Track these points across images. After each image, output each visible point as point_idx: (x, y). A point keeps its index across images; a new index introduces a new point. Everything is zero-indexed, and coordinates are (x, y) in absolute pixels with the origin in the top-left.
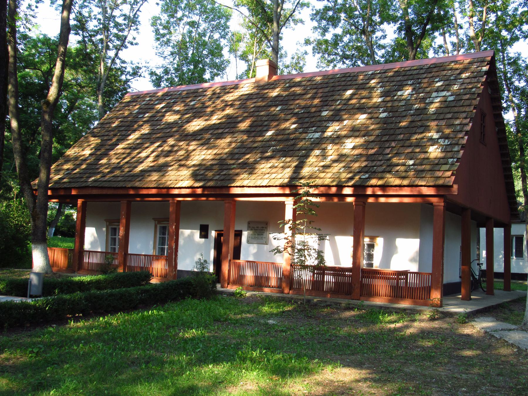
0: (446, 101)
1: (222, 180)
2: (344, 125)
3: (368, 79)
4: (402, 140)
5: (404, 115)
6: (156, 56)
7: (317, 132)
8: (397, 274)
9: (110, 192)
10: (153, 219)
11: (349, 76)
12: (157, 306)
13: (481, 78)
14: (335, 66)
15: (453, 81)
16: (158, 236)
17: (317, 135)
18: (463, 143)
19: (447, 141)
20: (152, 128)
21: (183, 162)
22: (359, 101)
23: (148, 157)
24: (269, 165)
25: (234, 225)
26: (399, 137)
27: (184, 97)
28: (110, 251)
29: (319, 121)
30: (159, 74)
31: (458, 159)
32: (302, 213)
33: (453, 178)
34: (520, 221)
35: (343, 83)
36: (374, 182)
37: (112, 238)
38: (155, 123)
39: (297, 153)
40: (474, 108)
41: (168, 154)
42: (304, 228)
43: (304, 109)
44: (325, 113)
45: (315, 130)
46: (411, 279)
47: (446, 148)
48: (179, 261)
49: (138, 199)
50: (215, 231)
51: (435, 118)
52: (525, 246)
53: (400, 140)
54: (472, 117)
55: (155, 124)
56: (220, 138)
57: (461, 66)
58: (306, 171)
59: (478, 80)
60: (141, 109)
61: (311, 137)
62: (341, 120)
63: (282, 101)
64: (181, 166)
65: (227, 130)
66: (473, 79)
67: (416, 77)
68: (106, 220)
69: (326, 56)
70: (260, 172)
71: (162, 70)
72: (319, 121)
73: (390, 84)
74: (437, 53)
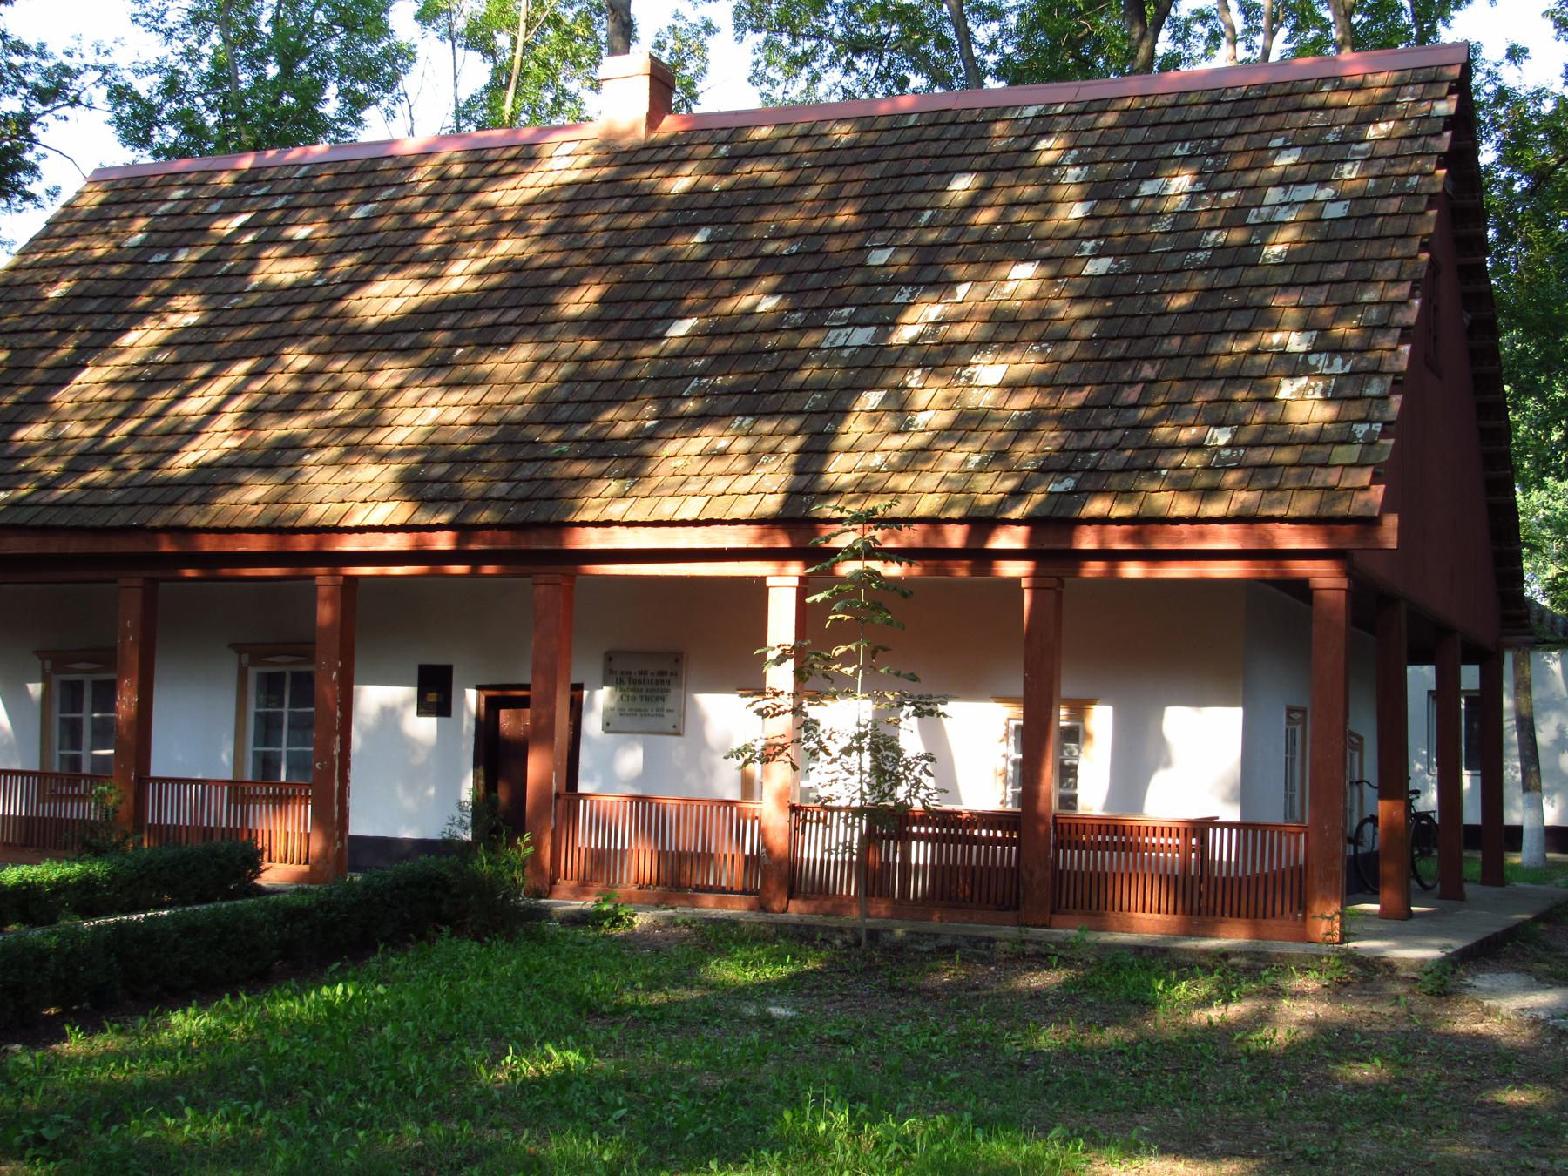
0: (1319, 220)
1: (522, 500)
2: (959, 299)
3: (1024, 135)
4: (1178, 356)
5: (1175, 265)
6: (137, 26)
7: (863, 325)
8: (1182, 833)
9: (75, 546)
10: (231, 646)
11: (953, 123)
12: (343, 968)
13: (1433, 141)
14: (815, 79)
15: (1335, 147)
16: (252, 709)
17: (861, 336)
18: (1396, 369)
19: (1338, 361)
20: (212, 305)
21: (356, 437)
22: (1003, 215)
23: (215, 412)
24: (697, 444)
25: (569, 667)
26: (1165, 346)
27: (324, 187)
28: (57, 769)
29: (862, 285)
30: (144, 94)
31: (1386, 424)
32: (847, 617)
33: (1378, 491)
34: (1531, 638)
35: (934, 148)
36: (1097, 507)
37: (63, 720)
38: (221, 285)
39: (794, 402)
40: (1424, 247)
41: (289, 406)
42: (856, 673)
43: (800, 240)
44: (879, 257)
45: (851, 315)
46: (1223, 846)
47: (1337, 388)
48: (354, 802)
49: (190, 573)
50: (479, 688)
51: (1287, 278)
53: (1172, 358)
54: (1416, 276)
55: (219, 289)
56: (490, 344)
57: (1358, 98)
58: (840, 469)
59: (1423, 147)
60: (156, 231)
61: (840, 342)
62: (944, 285)
63: (710, 208)
64: (351, 449)
65: (511, 316)
66: (1407, 143)
67: (1199, 129)
68: (43, 654)
69: (786, 40)
70: (665, 469)
71: (155, 80)
72: (862, 285)
73: (1110, 152)
74: (1182, 40)
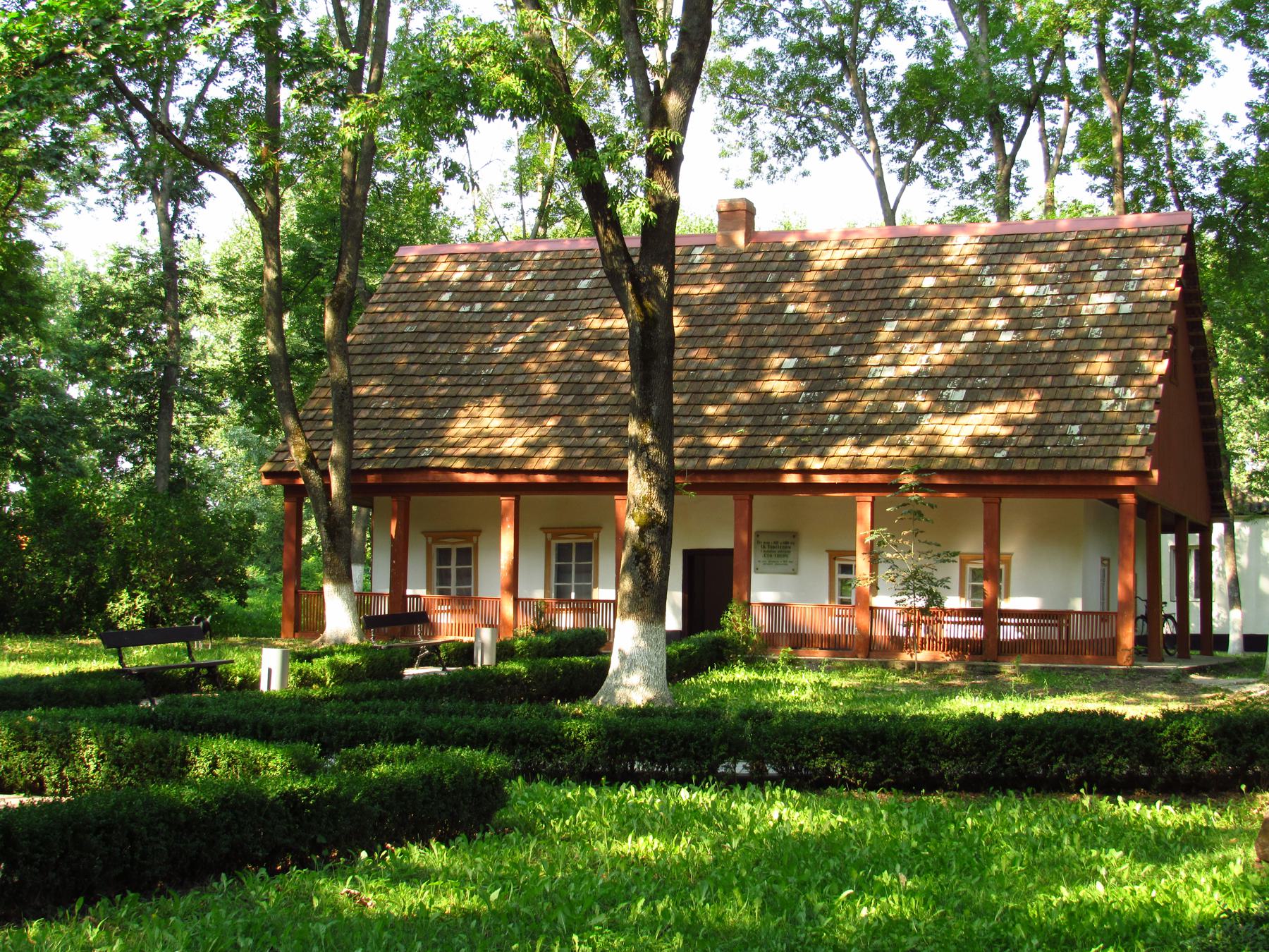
0: (1117, 314)
10: (542, 529)
16: (554, 563)
31: (1152, 425)
48: (480, 590)
52: (1219, 540)
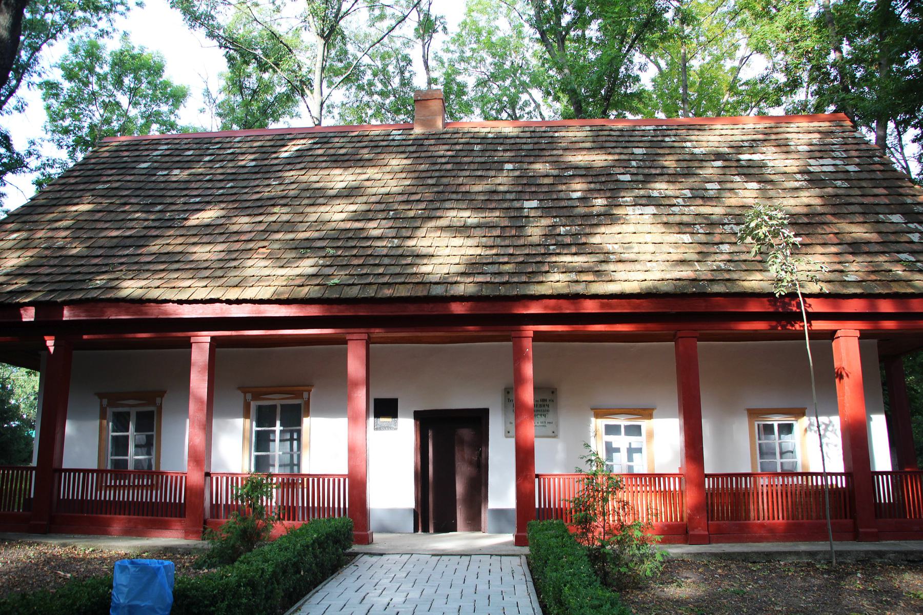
28: (109, 468)
